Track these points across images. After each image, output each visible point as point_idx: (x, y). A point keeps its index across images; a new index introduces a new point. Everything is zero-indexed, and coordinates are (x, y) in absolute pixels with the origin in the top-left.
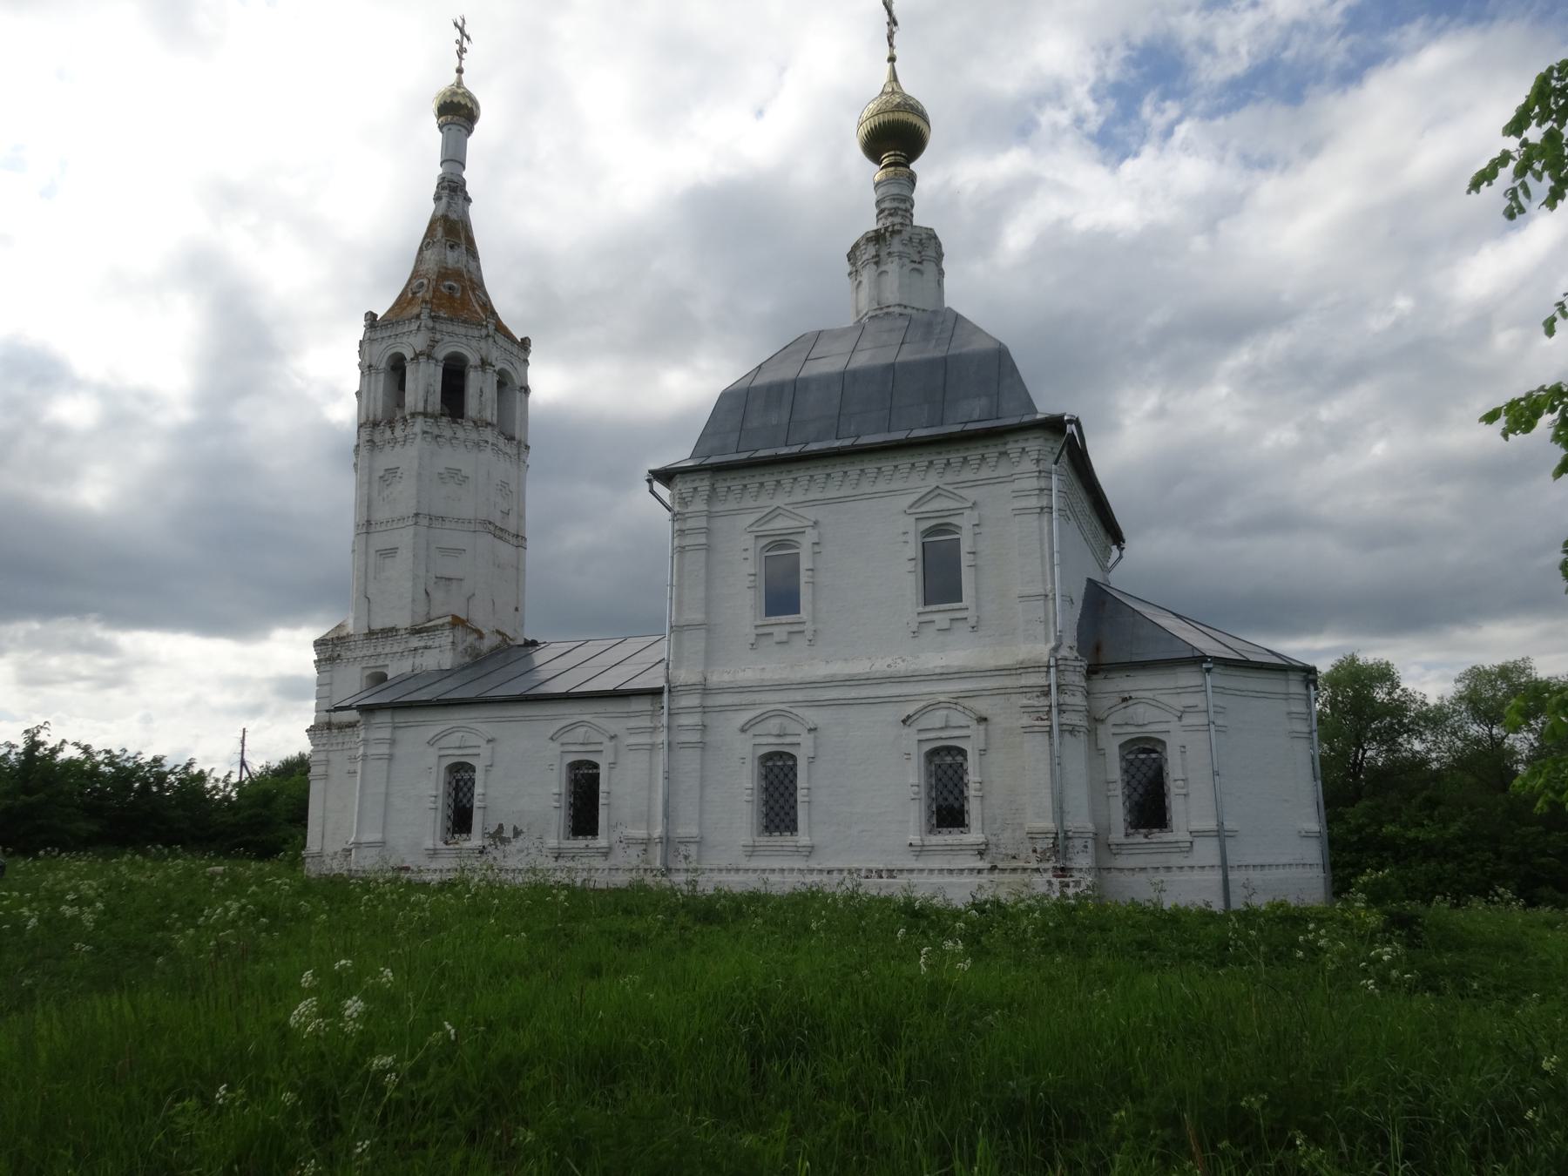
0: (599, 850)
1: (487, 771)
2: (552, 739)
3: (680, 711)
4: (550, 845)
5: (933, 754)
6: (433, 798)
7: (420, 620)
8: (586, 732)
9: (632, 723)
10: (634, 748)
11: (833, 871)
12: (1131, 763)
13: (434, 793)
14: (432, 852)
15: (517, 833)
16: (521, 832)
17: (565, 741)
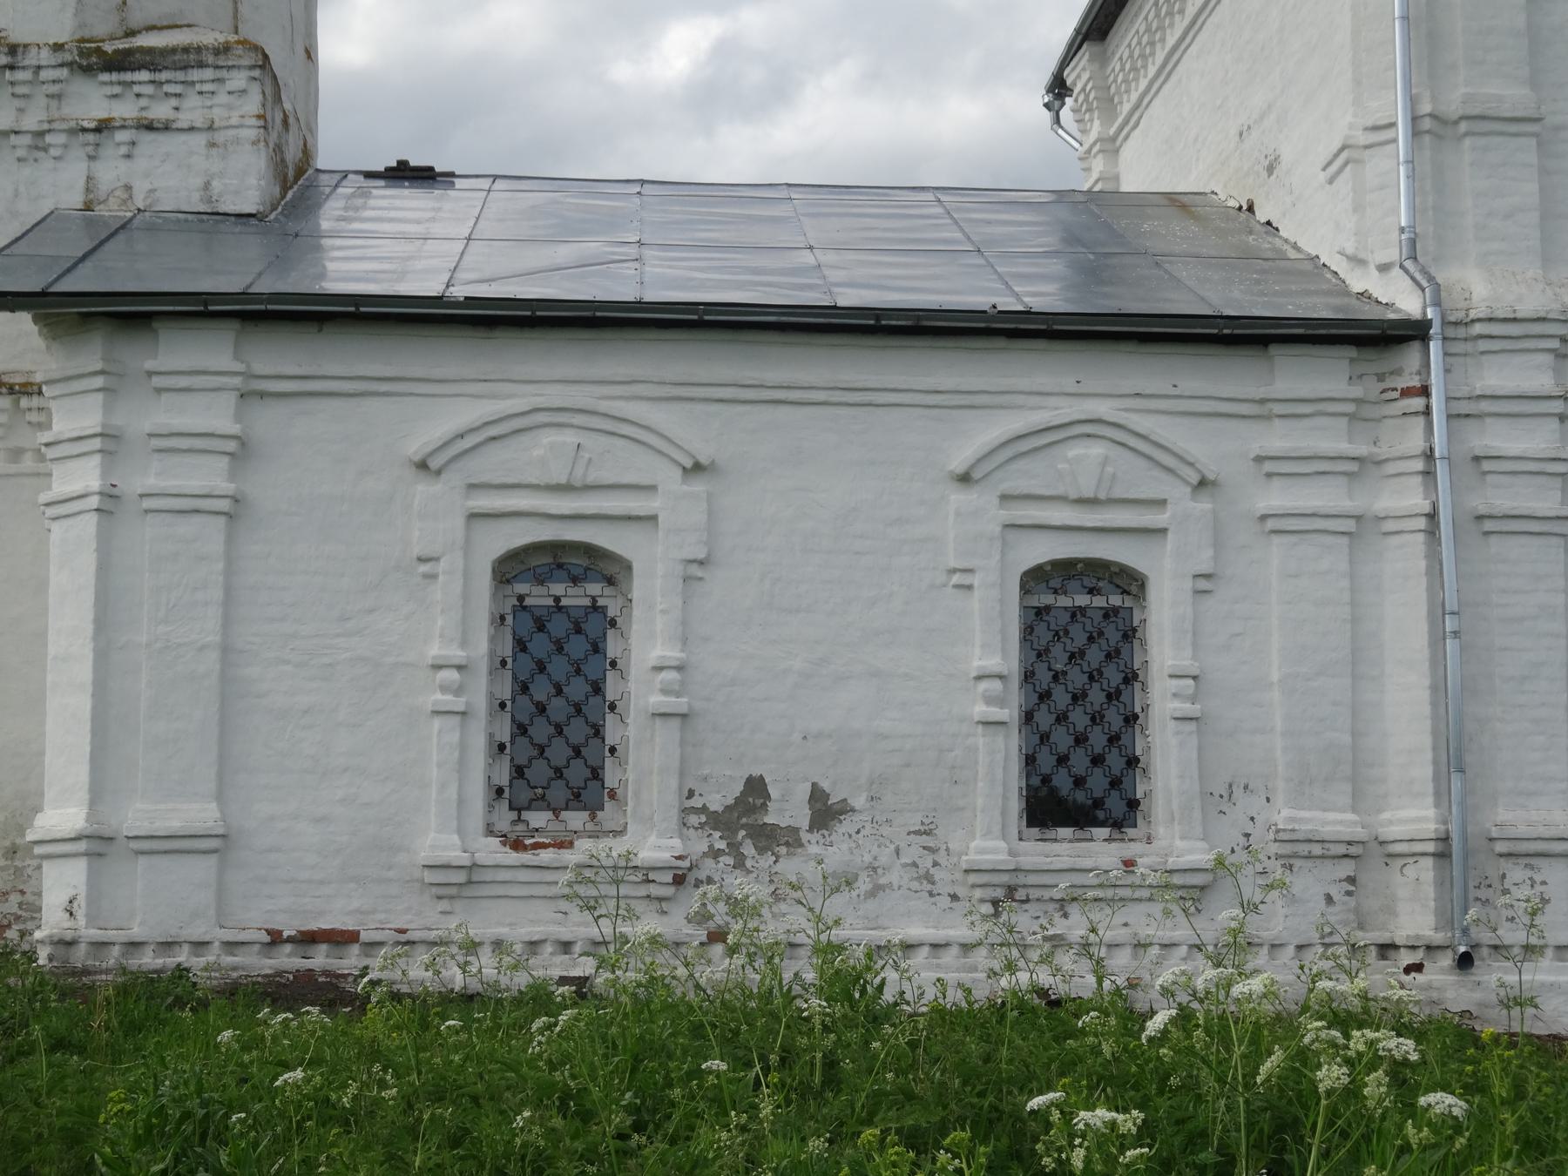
0: (1177, 880)
1: (687, 579)
2: (423, 466)
3: (1485, 406)
4: (973, 857)
5: (511, 567)
6: (453, 675)
7: (102, 26)
8: (1105, 461)
9: (1277, 438)
10: (1272, 524)
11: (179, 944)
12: (1041, 612)
13: (457, 654)
14: (460, 877)
15: (825, 812)
16: (844, 809)
17: (1008, 486)
